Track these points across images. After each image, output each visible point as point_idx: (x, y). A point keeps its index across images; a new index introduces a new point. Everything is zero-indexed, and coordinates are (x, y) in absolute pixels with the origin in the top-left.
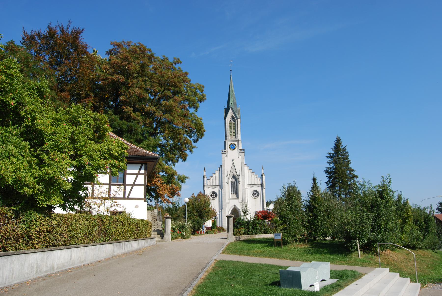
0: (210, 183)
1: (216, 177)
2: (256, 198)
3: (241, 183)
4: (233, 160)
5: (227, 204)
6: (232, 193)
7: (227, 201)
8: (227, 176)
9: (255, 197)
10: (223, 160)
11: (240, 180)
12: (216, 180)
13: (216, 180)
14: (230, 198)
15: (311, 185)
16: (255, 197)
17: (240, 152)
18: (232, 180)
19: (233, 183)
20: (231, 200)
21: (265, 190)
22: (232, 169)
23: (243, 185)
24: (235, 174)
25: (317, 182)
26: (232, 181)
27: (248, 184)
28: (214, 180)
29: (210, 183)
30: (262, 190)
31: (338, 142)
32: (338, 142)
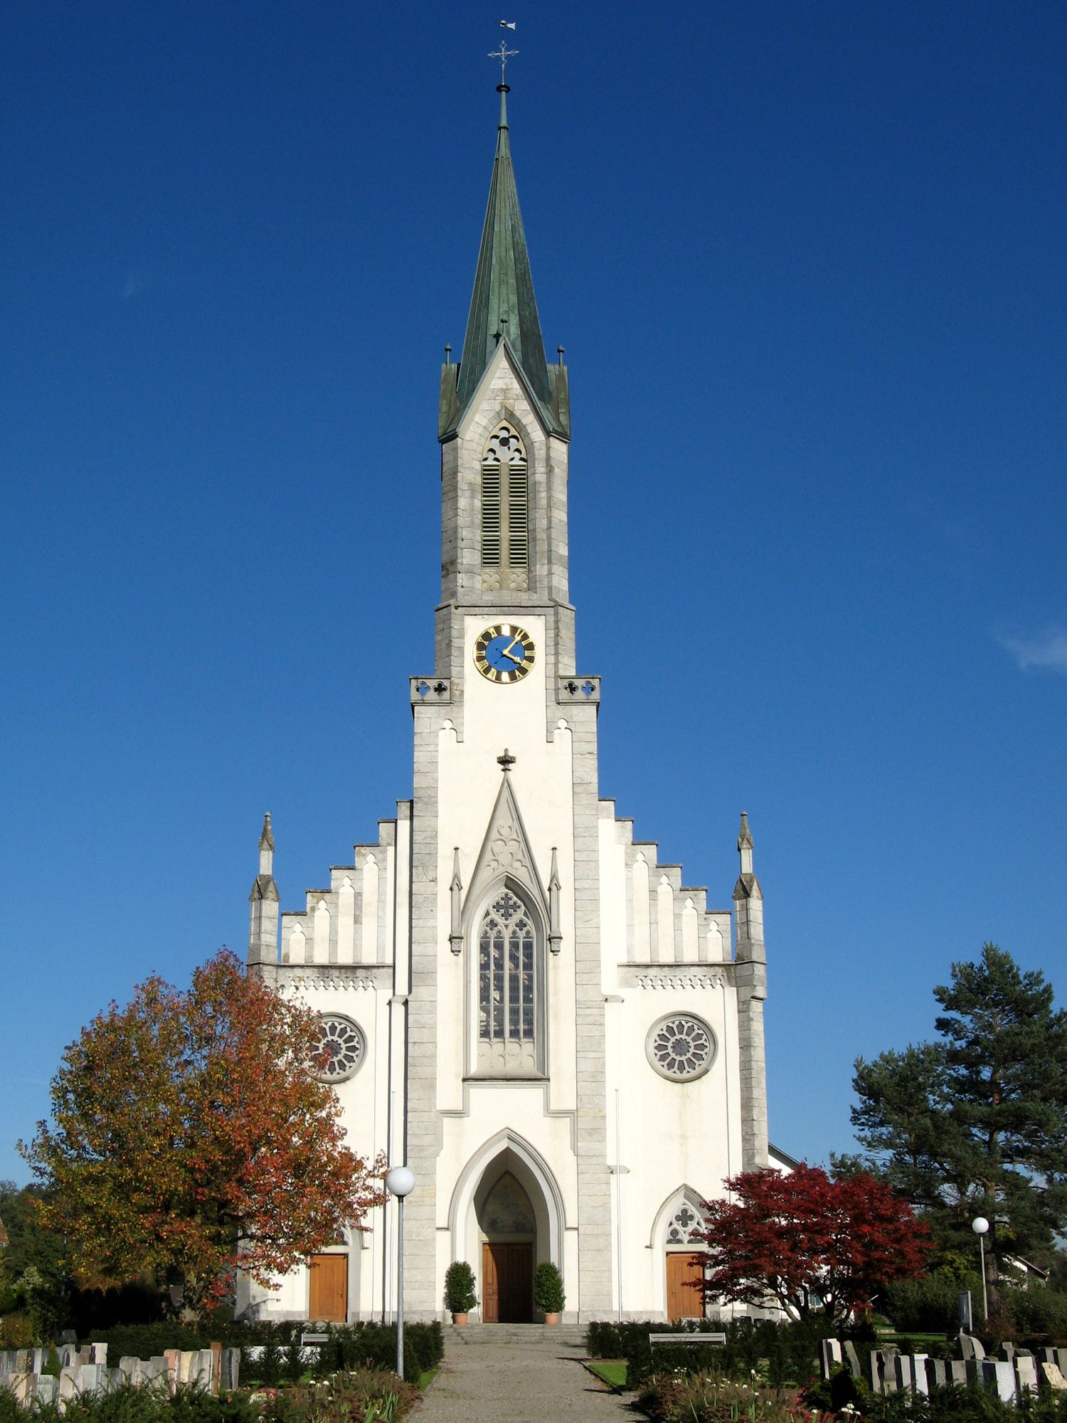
0: (309, 941)
1: (358, 895)
2: (685, 1075)
3: (566, 946)
4: (505, 761)
5: (447, 1122)
6: (485, 1033)
7: (448, 1092)
8: (455, 886)
9: (681, 1068)
10: (420, 756)
11: (565, 923)
12: (357, 920)
13: (357, 920)
14: (474, 1070)
15: (262, 831)
16: (681, 1068)
17: (565, 695)
18: (493, 924)
19: (499, 946)
20: (480, 1094)
21: (766, 1013)
22: (494, 835)
23: (587, 966)
24: (523, 876)
25: (193, 978)
26: (492, 935)
27: (625, 961)
28: (345, 921)
29: (309, 941)
30: (743, 1009)
31: (852, 1107)
32: (852, 1107)
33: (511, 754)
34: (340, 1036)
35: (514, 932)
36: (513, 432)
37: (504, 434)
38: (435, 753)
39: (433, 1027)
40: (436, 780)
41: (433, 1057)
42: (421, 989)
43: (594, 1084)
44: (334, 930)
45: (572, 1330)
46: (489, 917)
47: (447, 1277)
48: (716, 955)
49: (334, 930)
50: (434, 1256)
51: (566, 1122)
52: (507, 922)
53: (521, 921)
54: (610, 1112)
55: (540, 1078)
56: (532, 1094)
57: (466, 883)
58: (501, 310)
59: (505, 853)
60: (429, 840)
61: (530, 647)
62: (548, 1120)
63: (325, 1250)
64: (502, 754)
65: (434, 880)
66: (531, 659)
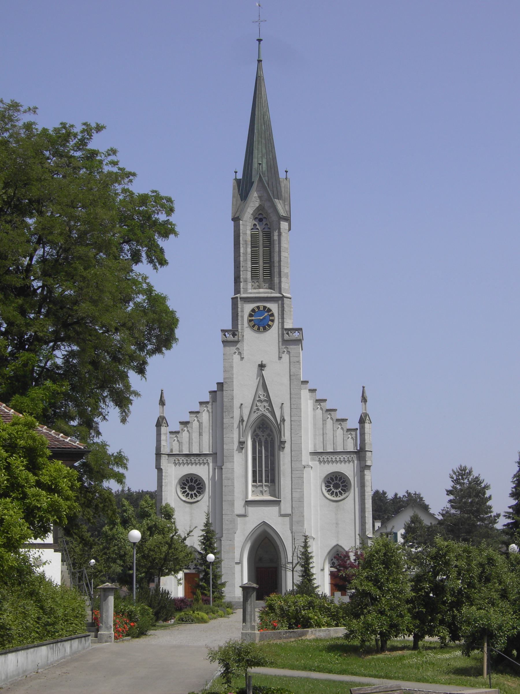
3: (287, 446)
11: (287, 436)
13: (200, 434)
20: (252, 510)
23: (295, 457)
28: (195, 436)
33: (264, 363)
34: (195, 483)
35: (266, 439)
36: (264, 216)
37: (260, 217)
38: (232, 391)
39: (233, 479)
40: (233, 374)
41: (233, 491)
42: (227, 464)
43: (299, 503)
44: (190, 439)
45: (58, 443)
46: (256, 432)
47: (173, 312)
48: (351, 447)
49: (190, 439)
50: (234, 573)
51: (287, 519)
52: (263, 434)
53: (269, 433)
54: (306, 514)
55: (277, 503)
56: (274, 509)
57: (245, 419)
58: (259, 156)
59: (263, 409)
60: (230, 400)
61: (272, 315)
62: (281, 518)
63: (98, 587)
64: (260, 363)
65: (232, 418)
66: (273, 321)
